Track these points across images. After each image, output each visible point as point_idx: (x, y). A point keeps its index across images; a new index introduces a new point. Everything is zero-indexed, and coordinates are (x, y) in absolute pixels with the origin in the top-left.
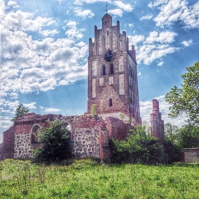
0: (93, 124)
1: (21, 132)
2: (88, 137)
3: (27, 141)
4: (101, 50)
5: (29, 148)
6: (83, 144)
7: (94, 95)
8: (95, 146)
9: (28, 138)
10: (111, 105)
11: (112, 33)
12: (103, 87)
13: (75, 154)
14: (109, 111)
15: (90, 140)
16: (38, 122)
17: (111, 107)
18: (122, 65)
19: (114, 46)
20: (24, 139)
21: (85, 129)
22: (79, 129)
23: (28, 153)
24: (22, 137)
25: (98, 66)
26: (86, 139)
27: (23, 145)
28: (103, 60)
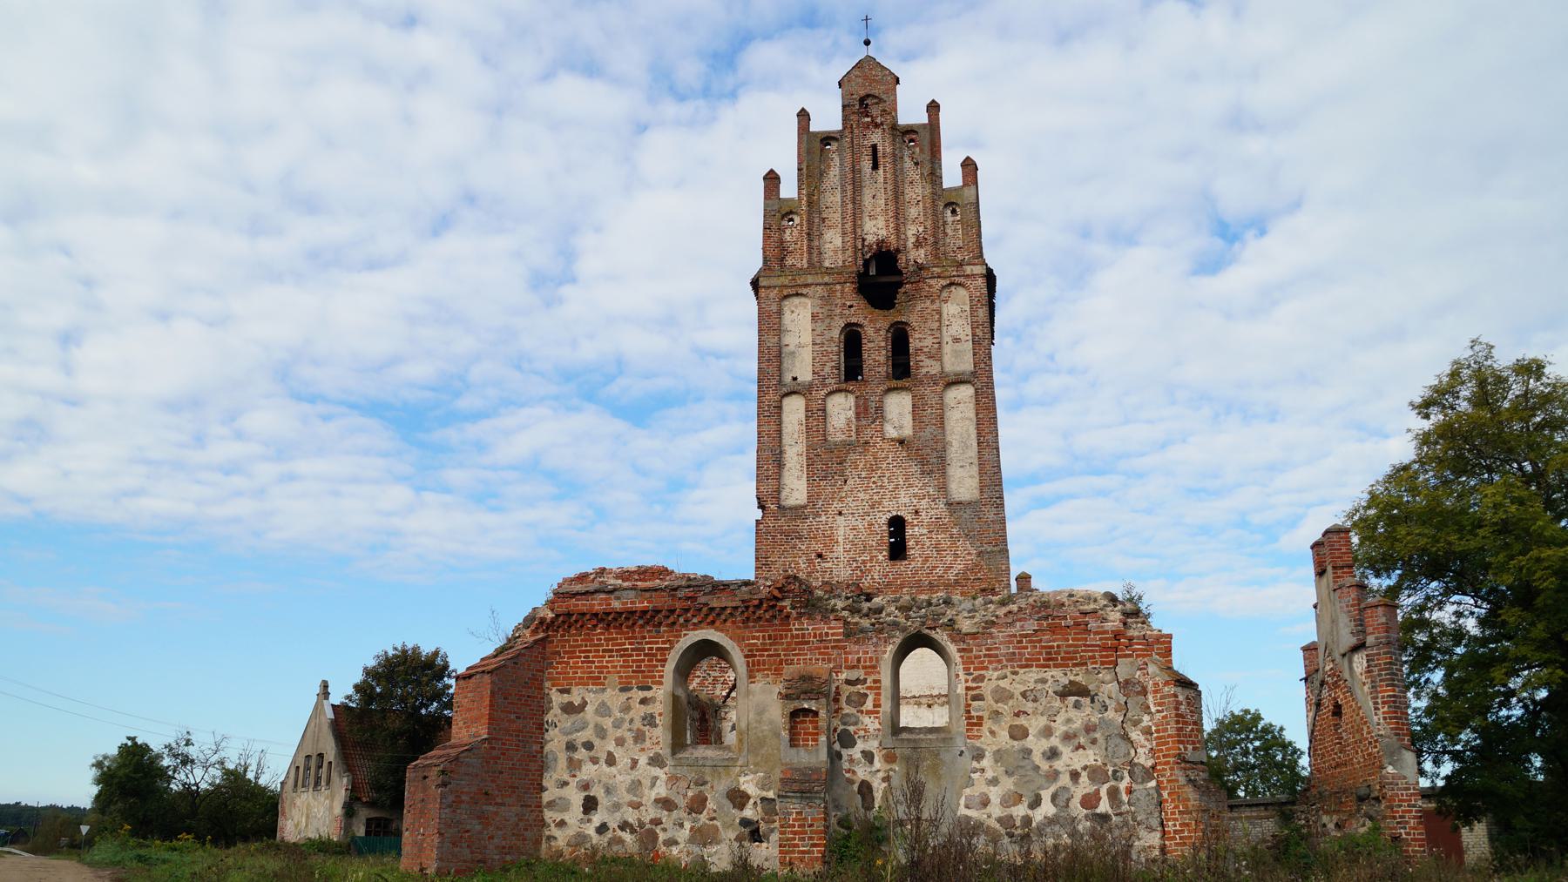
0: (1105, 648)
1: (597, 681)
2: (1078, 725)
3: (639, 737)
4: (833, 242)
5: (656, 778)
6: (1045, 766)
7: (796, 489)
8: (1127, 779)
9: (650, 720)
10: (898, 550)
11: (896, 159)
12: (848, 446)
13: (998, 826)
14: (889, 584)
15: (1094, 742)
16: (713, 617)
17: (901, 566)
18: (963, 337)
19: (912, 231)
20: (617, 725)
21: (1057, 673)
22: (1016, 673)
23: (650, 813)
24: (603, 710)
25: (820, 327)
26: (1067, 737)
27: (611, 760)
28: (847, 293)
